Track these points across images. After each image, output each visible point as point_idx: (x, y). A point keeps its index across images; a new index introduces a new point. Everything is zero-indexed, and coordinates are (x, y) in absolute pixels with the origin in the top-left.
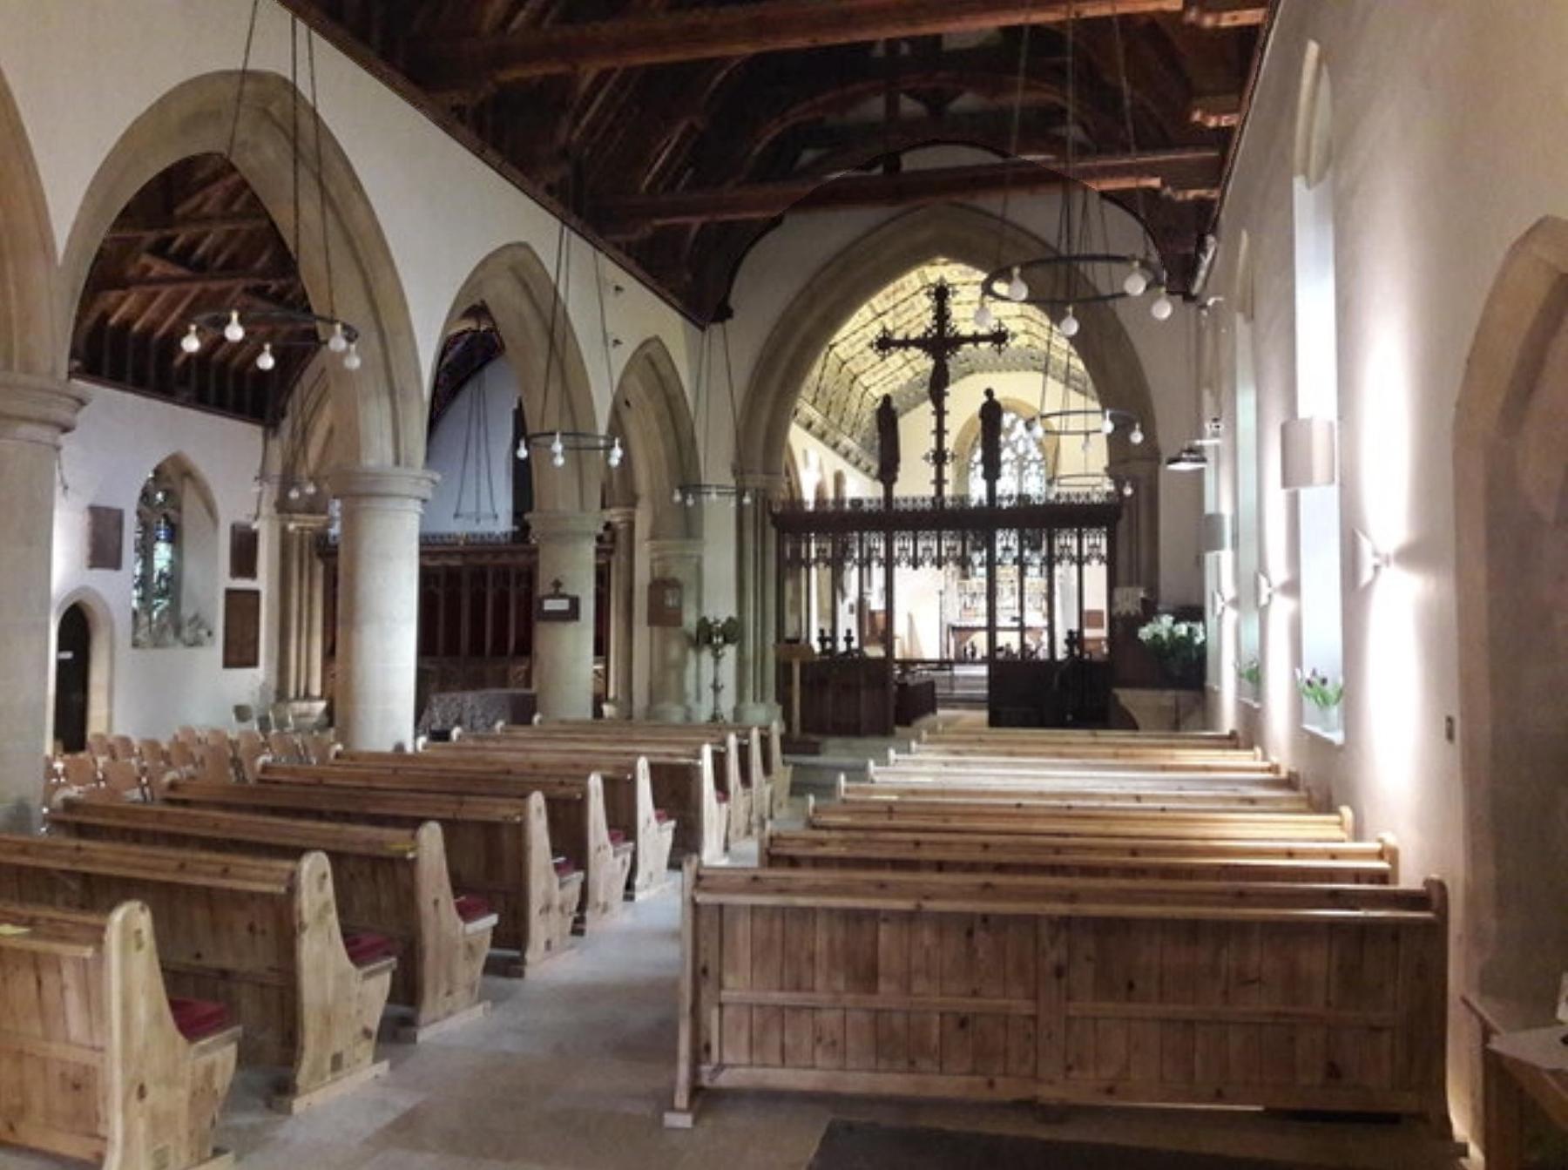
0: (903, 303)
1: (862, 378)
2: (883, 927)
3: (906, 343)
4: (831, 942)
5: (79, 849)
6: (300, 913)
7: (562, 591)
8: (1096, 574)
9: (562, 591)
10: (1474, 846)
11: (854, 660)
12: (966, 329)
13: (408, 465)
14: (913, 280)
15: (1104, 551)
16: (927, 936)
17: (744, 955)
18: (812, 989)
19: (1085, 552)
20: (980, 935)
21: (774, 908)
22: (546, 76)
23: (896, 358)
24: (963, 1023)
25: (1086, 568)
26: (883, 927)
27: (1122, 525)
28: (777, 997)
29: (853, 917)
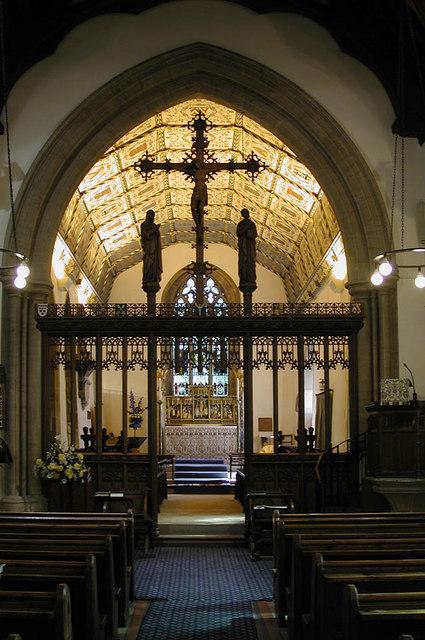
0: (168, 132)
1: (100, 231)
3: (168, 167)
8: (339, 377)
10: (53, 386)
11: (127, 444)
12: (223, 159)
14: (180, 113)
19: (104, 358)
22: (62, 603)
23: (158, 178)
25: (306, 372)
27: (363, 333)
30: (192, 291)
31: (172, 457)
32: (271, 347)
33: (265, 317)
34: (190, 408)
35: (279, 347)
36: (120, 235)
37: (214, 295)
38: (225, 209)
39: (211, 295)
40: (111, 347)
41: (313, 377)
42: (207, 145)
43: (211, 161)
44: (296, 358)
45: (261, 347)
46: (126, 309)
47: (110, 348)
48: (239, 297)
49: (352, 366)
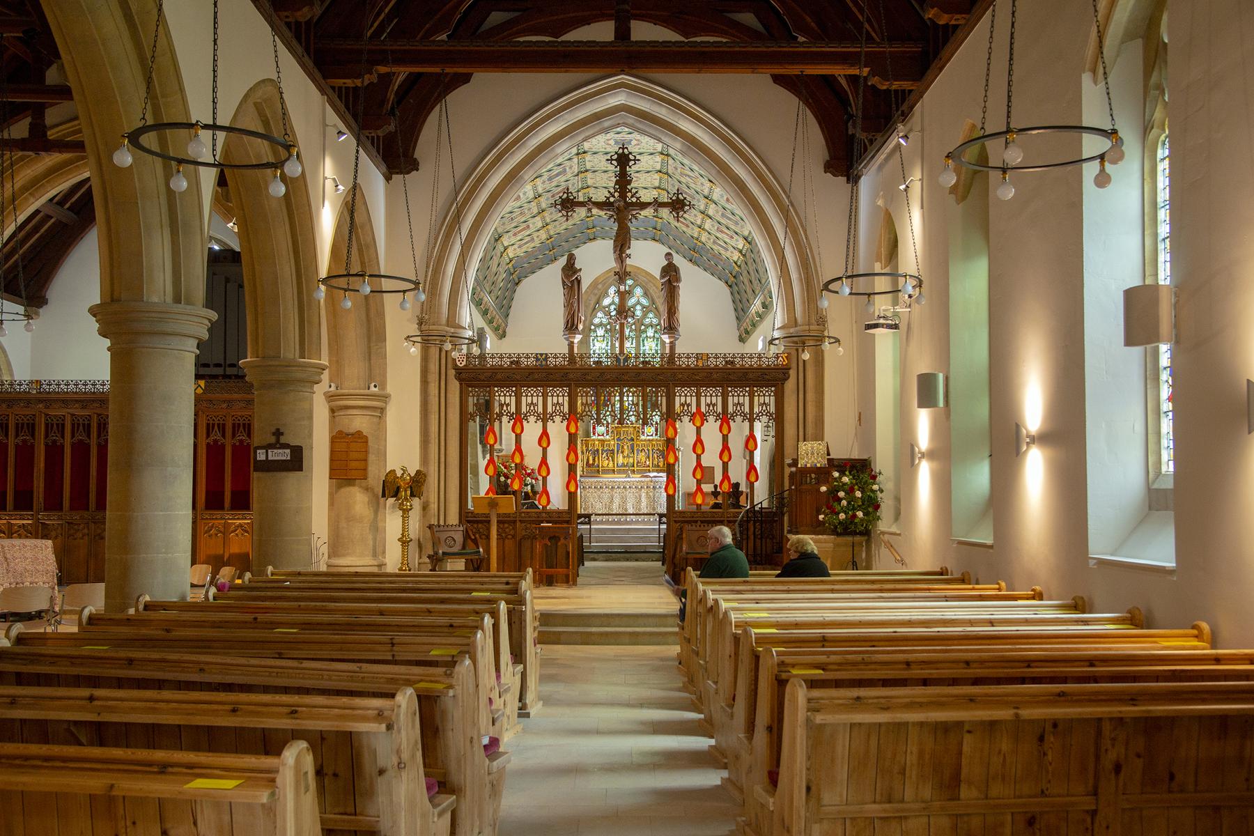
2: (968, 739)
4: (921, 754)
5: (91, 699)
6: (374, 753)
7: (283, 440)
9: (283, 440)
12: (646, 196)
13: (189, 303)
15: (772, 409)
16: (1005, 745)
17: (842, 772)
18: (902, 801)
20: (1050, 738)
21: (871, 725)
24: (1031, 822)
26: (968, 739)
27: (790, 385)
28: (873, 809)
29: (945, 728)
30: (613, 303)
31: (589, 516)
32: (694, 399)
33: (688, 368)
34: (611, 453)
35: (703, 399)
36: (528, 239)
37: (644, 307)
38: (657, 176)
39: (638, 307)
40: (532, 398)
41: (739, 430)
42: (629, 182)
43: (634, 200)
44: (720, 410)
45: (684, 398)
46: (546, 359)
47: (529, 399)
48: (595, 568)
49: (778, 419)
